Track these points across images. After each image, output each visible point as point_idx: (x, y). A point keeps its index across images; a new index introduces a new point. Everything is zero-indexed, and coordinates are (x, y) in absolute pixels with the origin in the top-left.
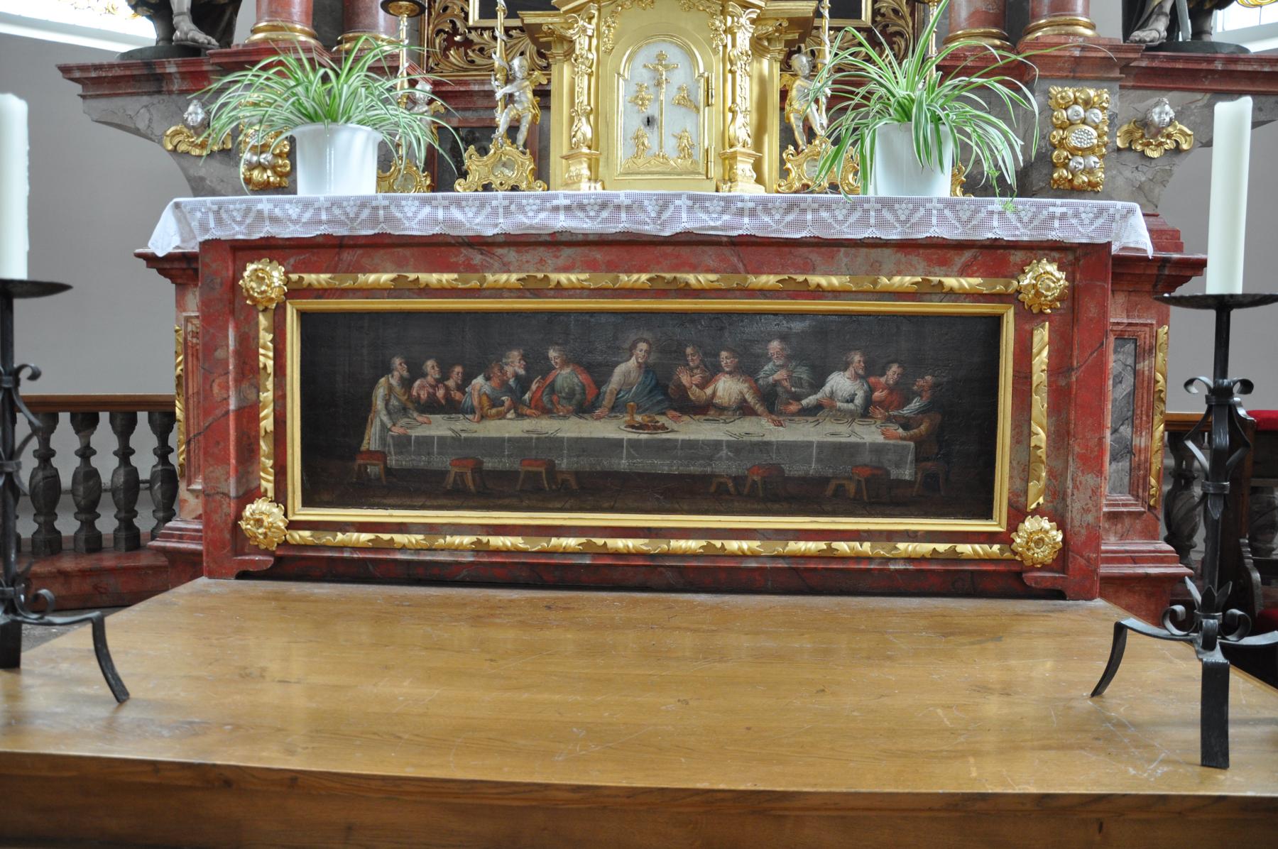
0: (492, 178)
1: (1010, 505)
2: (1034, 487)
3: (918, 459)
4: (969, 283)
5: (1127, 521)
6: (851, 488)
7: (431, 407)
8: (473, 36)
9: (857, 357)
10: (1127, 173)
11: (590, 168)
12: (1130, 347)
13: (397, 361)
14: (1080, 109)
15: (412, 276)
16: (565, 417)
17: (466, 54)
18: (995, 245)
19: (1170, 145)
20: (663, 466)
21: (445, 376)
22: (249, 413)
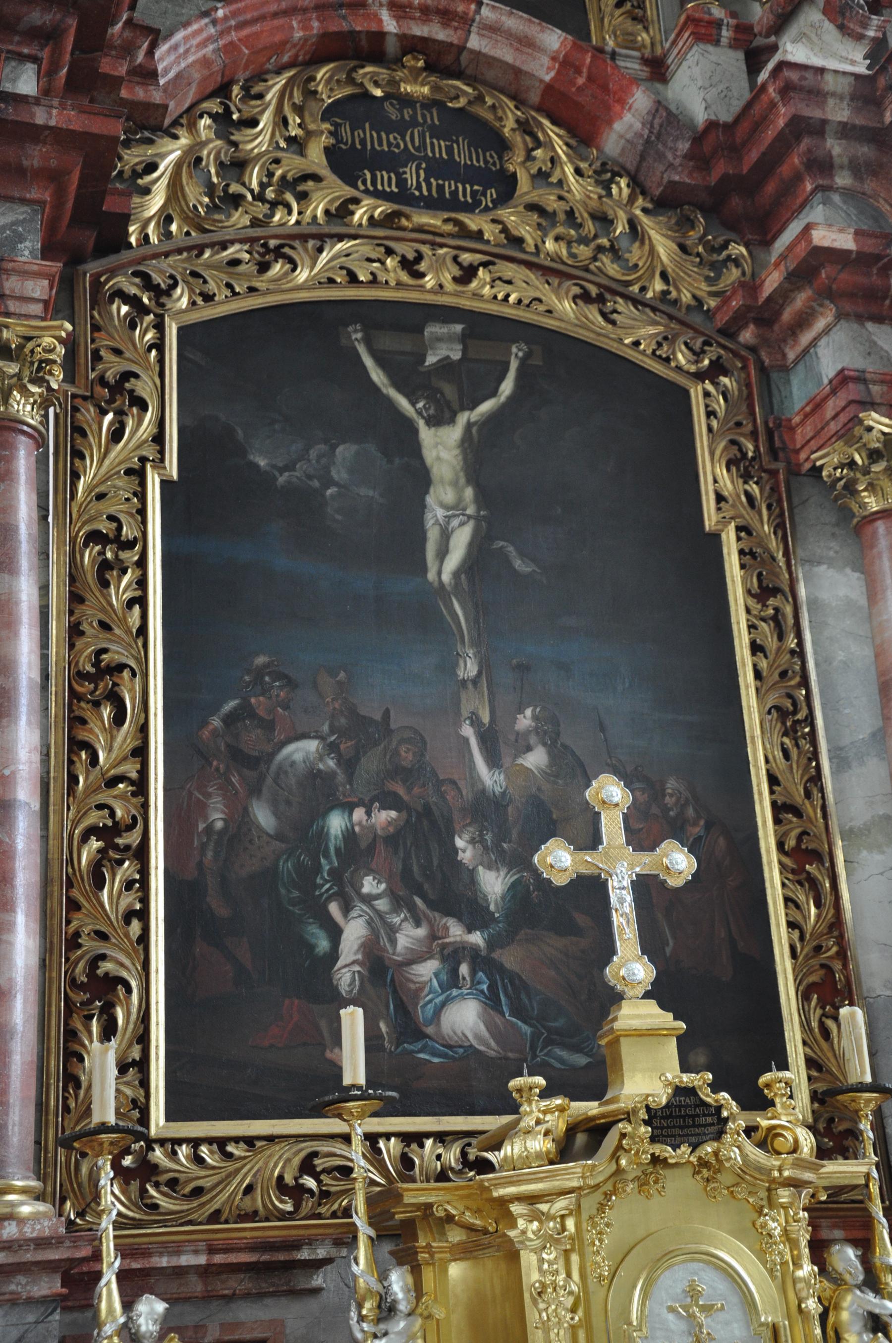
8: (158, 1154)
17: (143, 1192)
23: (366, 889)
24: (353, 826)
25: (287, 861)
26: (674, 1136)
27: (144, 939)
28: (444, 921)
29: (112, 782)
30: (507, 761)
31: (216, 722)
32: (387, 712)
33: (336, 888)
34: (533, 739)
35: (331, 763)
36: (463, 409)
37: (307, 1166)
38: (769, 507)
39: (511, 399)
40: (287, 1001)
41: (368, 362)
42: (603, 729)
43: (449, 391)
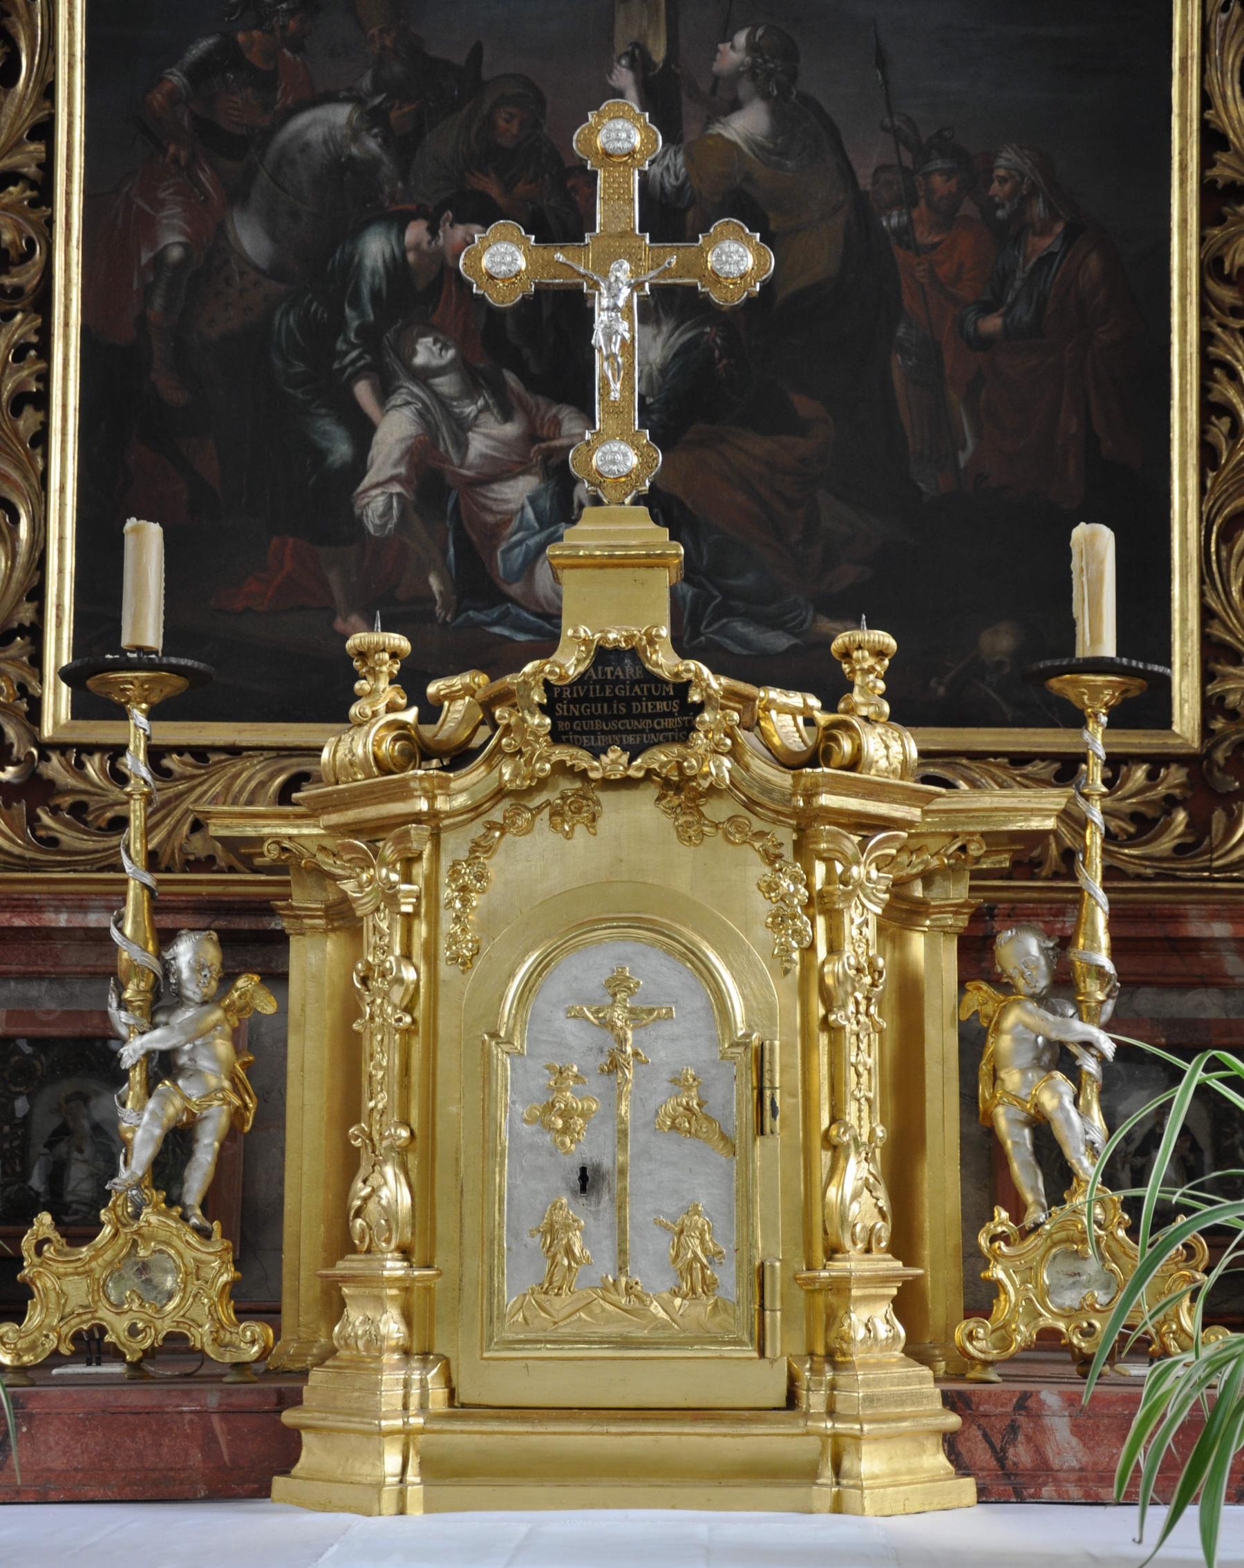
0: (105, 1314)
8: (55, 768)
11: (407, 1318)
17: (33, 820)
23: (420, 360)
24: (404, 253)
25: (286, 313)
26: (594, 733)
27: (41, 439)
28: (554, 411)
30: (691, 131)
31: (176, 78)
32: (476, 53)
33: (368, 358)
35: (372, 145)
40: (275, 541)
42: (881, 61)
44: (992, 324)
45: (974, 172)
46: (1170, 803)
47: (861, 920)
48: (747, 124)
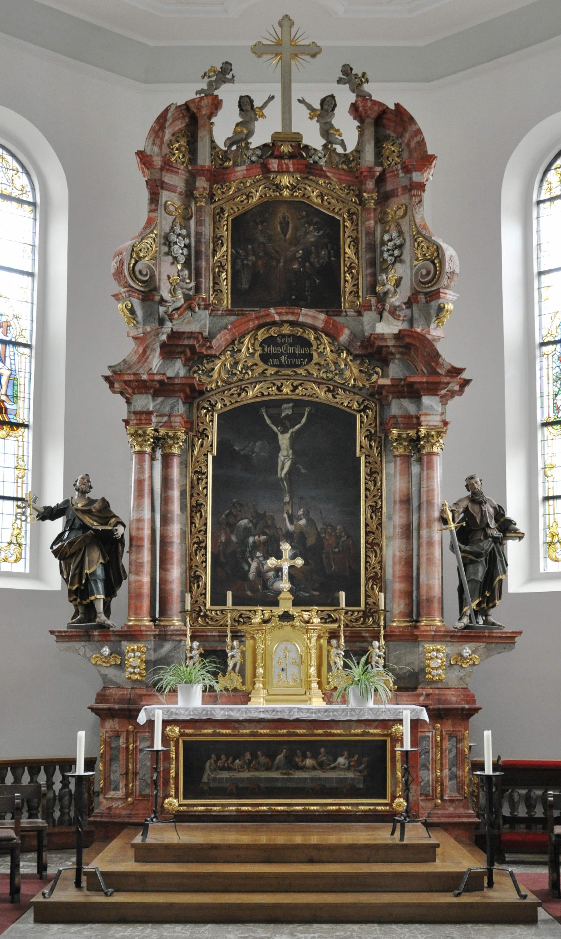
1: (391, 795)
2: (398, 789)
3: (364, 782)
4: (376, 731)
5: (457, 802)
6: (345, 791)
7: (223, 769)
8: (208, 613)
9: (346, 753)
10: (456, 673)
12: (454, 739)
13: (213, 756)
14: (435, 653)
15: (218, 731)
16: (263, 771)
18: (384, 720)
19: (472, 662)
20: (290, 785)
21: (227, 759)
22: (167, 771)
27: (206, 567)
29: (200, 531)
30: (295, 523)
32: (265, 512)
34: (302, 517)
36: (291, 428)
37: (240, 616)
38: (377, 448)
39: (304, 424)
41: (266, 417)
43: (287, 423)
44: (337, 550)
45: (334, 529)
46: (361, 617)
47: (314, 640)
48: (303, 522)
